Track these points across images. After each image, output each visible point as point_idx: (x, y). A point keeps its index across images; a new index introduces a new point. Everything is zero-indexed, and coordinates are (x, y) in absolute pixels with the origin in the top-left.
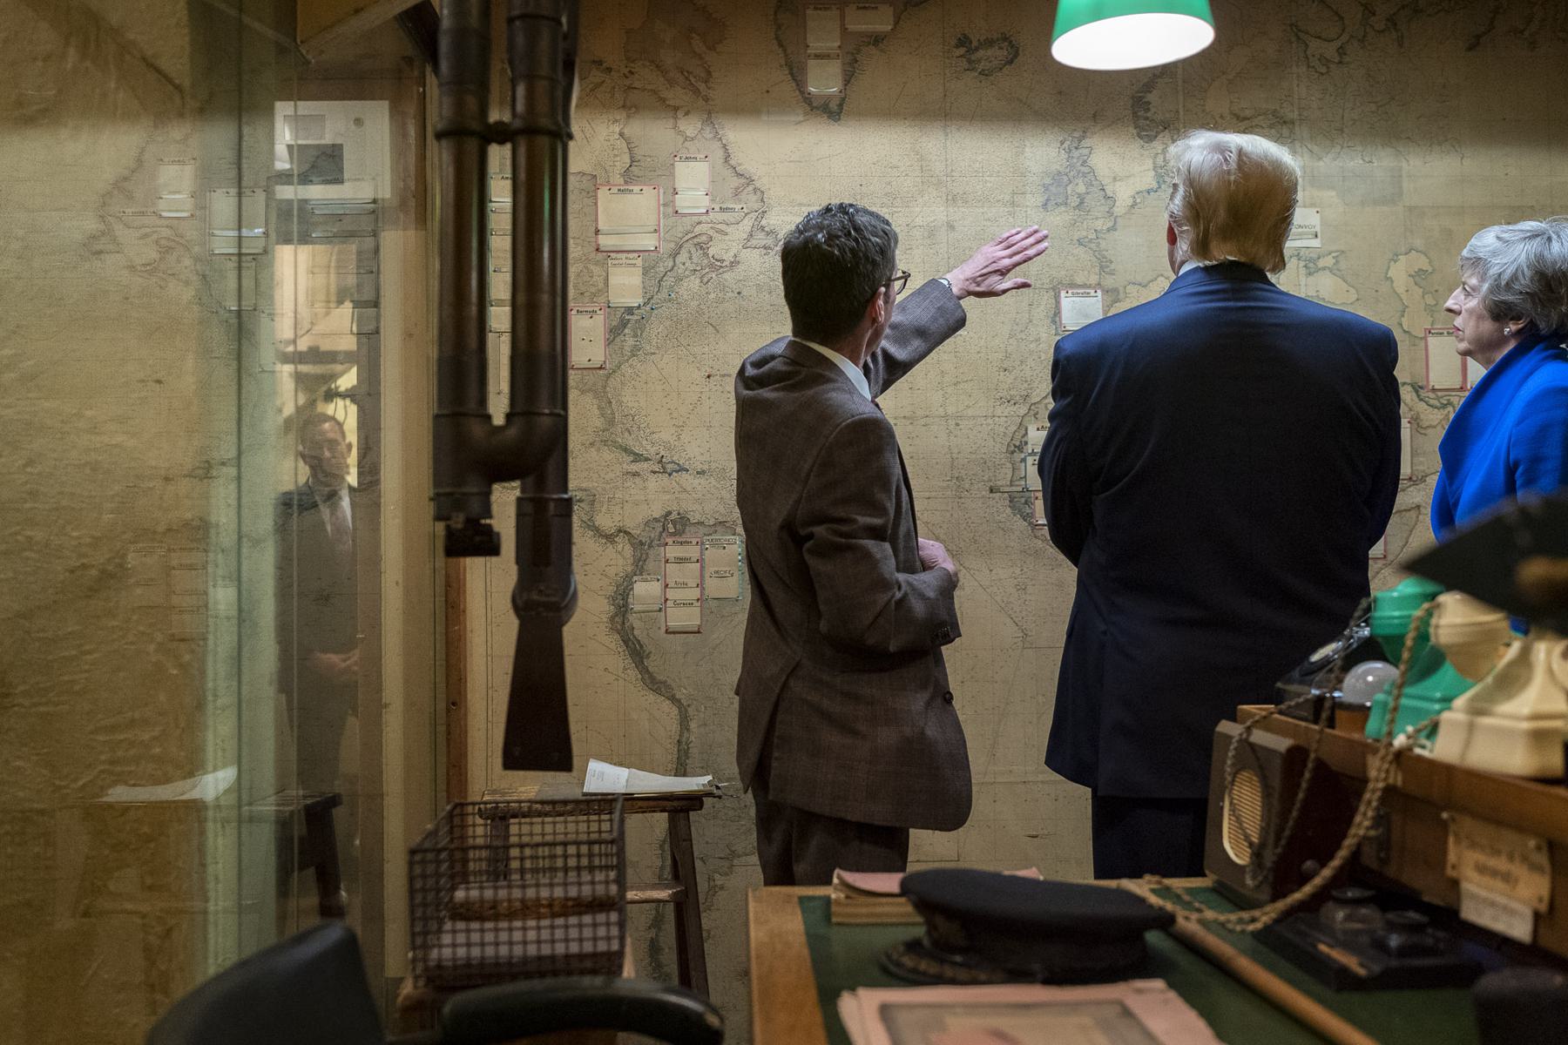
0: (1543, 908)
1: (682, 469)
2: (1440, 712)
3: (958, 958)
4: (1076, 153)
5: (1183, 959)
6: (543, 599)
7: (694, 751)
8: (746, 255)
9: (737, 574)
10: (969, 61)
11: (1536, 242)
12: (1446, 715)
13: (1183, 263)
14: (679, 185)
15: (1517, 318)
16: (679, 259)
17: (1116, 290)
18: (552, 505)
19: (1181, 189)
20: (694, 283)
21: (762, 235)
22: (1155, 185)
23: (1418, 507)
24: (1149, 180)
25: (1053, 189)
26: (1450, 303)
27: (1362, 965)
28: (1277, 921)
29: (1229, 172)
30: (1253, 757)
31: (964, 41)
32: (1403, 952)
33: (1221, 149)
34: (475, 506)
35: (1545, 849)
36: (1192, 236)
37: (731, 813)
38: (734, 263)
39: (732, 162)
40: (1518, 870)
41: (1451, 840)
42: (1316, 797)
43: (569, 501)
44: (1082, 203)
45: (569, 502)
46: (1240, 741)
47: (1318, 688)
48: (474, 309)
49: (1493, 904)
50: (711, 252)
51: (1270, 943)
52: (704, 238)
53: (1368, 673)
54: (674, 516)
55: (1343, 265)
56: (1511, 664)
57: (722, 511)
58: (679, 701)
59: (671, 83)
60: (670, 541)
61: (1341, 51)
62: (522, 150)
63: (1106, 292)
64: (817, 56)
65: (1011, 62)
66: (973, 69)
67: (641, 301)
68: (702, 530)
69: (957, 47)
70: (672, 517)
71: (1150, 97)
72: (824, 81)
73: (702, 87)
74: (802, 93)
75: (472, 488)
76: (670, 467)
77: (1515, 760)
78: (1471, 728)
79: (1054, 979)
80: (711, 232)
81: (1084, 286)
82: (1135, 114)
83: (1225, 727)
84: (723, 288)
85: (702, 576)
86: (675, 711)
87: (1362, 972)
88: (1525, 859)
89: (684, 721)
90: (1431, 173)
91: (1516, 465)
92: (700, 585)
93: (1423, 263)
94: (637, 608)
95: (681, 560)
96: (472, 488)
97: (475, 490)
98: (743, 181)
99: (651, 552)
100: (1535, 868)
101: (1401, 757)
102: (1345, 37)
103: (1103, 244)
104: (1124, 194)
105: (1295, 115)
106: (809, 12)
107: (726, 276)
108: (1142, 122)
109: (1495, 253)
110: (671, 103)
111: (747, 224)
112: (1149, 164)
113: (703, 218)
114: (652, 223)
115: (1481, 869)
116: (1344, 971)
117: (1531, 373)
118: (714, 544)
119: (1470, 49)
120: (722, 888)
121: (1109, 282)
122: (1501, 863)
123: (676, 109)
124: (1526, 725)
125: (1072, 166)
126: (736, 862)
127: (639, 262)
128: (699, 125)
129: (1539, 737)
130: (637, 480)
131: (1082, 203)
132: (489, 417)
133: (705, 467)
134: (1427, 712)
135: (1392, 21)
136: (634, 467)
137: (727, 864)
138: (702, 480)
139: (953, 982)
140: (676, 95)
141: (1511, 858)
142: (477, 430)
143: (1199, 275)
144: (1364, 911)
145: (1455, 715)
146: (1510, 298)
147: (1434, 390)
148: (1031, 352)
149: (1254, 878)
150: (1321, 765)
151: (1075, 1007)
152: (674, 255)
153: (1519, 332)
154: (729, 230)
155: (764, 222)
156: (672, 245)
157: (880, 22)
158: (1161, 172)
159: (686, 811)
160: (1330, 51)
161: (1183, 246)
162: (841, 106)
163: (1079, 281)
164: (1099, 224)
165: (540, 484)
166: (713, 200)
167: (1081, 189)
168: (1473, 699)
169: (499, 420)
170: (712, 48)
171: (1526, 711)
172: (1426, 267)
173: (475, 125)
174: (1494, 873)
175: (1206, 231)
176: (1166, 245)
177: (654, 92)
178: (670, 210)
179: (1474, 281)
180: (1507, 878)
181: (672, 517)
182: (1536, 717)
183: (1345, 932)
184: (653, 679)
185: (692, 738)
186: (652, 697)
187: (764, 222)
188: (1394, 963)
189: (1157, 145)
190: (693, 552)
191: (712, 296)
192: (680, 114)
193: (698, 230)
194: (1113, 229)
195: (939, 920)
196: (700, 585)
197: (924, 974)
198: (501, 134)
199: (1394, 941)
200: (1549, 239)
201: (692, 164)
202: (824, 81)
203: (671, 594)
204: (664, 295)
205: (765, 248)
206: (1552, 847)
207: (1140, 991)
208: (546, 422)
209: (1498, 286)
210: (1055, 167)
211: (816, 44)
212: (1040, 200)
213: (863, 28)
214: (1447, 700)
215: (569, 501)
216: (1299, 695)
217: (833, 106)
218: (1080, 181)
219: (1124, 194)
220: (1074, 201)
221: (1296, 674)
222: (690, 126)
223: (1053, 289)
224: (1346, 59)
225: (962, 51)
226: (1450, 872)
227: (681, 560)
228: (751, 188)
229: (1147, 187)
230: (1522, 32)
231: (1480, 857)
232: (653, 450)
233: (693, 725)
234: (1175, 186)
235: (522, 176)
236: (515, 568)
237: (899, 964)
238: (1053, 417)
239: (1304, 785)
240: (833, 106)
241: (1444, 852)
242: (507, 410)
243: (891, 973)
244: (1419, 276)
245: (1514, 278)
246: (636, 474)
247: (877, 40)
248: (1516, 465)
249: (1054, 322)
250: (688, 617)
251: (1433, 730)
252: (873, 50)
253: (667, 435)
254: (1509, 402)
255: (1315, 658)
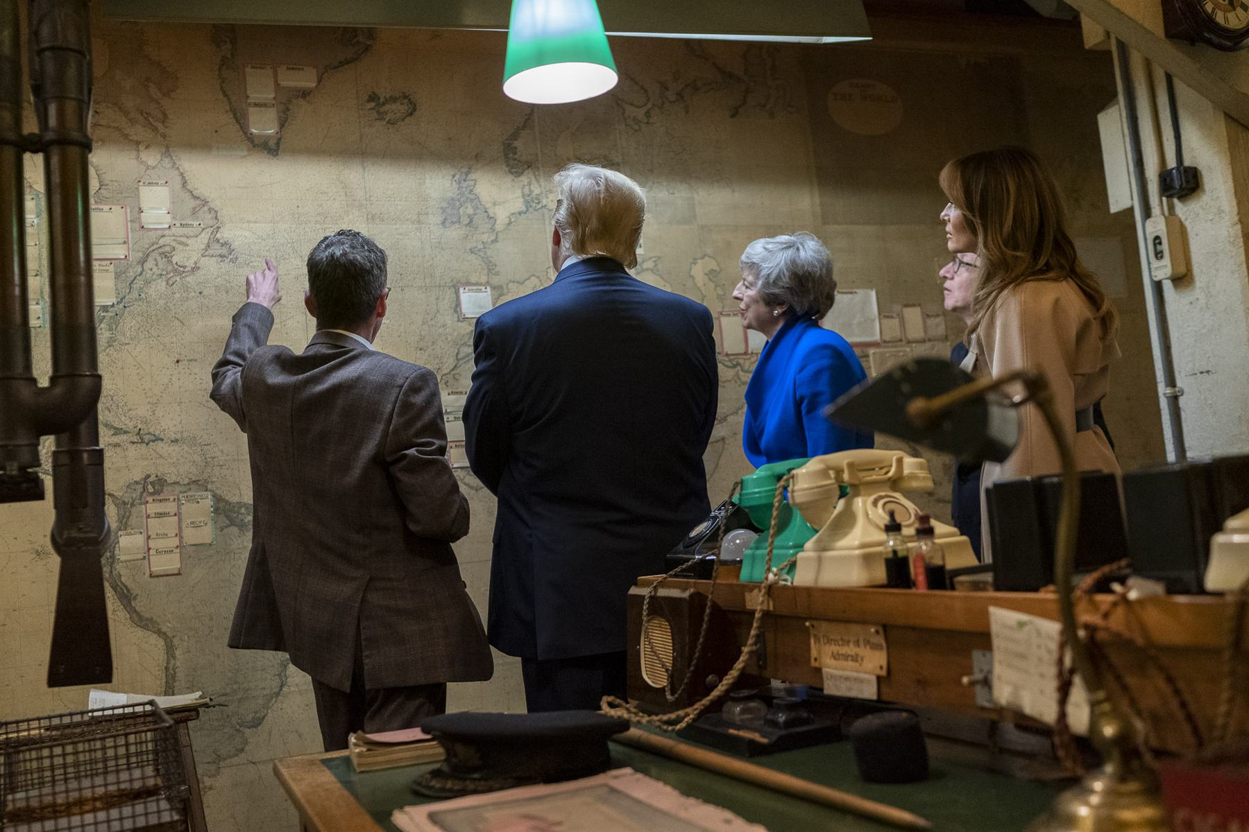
0: (884, 673)
1: (158, 439)
2: (796, 554)
3: (476, 776)
4: (464, 184)
5: (636, 754)
6: (82, 535)
7: (180, 675)
8: (204, 262)
9: (210, 523)
10: (378, 113)
11: (790, 252)
12: (800, 555)
13: (566, 258)
14: (144, 206)
15: (781, 304)
16: (148, 265)
17: (500, 287)
18: (85, 456)
19: (565, 205)
20: (161, 285)
21: (218, 246)
22: (524, 208)
23: (723, 439)
24: (519, 205)
25: (449, 211)
26: (736, 293)
27: (764, 737)
28: (699, 716)
29: (599, 192)
30: (659, 607)
31: (373, 98)
32: (788, 724)
33: (594, 177)
34: (25, 457)
35: (881, 632)
36: (573, 236)
37: (216, 724)
38: (195, 269)
39: (189, 187)
40: (864, 651)
41: (812, 641)
42: (713, 631)
43: (102, 450)
44: (471, 221)
45: (100, 453)
46: (651, 597)
47: (699, 554)
48: (17, 291)
49: (847, 679)
50: (175, 260)
51: (692, 734)
52: (167, 249)
53: (736, 537)
54: (152, 478)
55: (660, 266)
56: (840, 514)
57: (194, 470)
58: (165, 634)
59: (133, 122)
60: (150, 499)
61: (648, 114)
62: (55, 160)
63: (494, 288)
64: (256, 105)
65: (411, 114)
66: (383, 119)
67: (115, 301)
68: (178, 489)
69: (369, 101)
70: (151, 479)
71: (516, 144)
72: (264, 125)
73: (160, 126)
74: (245, 133)
75: (22, 441)
76: (146, 438)
77: (854, 576)
78: (820, 560)
79: (549, 779)
80: (173, 244)
81: (476, 284)
82: (506, 155)
83: (634, 591)
84: (186, 289)
85: (180, 528)
86: (161, 643)
87: (765, 741)
88: (867, 642)
89: (170, 650)
90: (714, 202)
91: (802, 399)
92: (179, 535)
93: (713, 265)
94: (123, 558)
95: (160, 515)
96: (22, 441)
97: (25, 442)
98: (198, 202)
99: (134, 510)
100: (875, 647)
101: (771, 590)
102: (649, 106)
103: (489, 253)
104: (502, 214)
105: (619, 159)
106: (248, 70)
107: (188, 279)
108: (511, 162)
109: (764, 260)
110: (135, 138)
111: (204, 237)
112: (519, 193)
113: (166, 232)
114: (121, 236)
115: (836, 657)
116: (752, 742)
117: (799, 338)
118: (189, 499)
119: (733, 116)
120: (210, 788)
121: (495, 281)
122: (851, 650)
123: (138, 143)
124: (857, 552)
125: (462, 194)
126: (222, 764)
127: (111, 268)
128: (159, 157)
129: (868, 559)
130: (118, 450)
131: (471, 221)
132: (34, 381)
133: (178, 436)
134: (786, 556)
135: (680, 95)
136: (116, 439)
137: (213, 767)
138: (176, 448)
139: (475, 792)
140: (138, 132)
141: (857, 644)
142: (25, 392)
143: (581, 268)
144: (752, 704)
145: (809, 551)
146: (776, 291)
147: (727, 355)
148: (440, 335)
149: (672, 694)
150: (715, 607)
151: (576, 792)
152: (142, 262)
153: (784, 313)
154: (189, 242)
155: (218, 236)
156: (140, 254)
157: (305, 79)
158: (531, 203)
159: (186, 720)
160: (640, 113)
161: (566, 244)
162: (278, 144)
163: (473, 280)
164: (485, 237)
165: (75, 438)
166: (174, 218)
167: (470, 211)
168: (818, 541)
169: (44, 382)
170: (167, 94)
171: (857, 543)
172: (716, 268)
173: (11, 135)
174: (846, 657)
175: (584, 232)
176: (550, 245)
177: (118, 129)
178: (137, 226)
179: (750, 278)
180: (855, 658)
181: (151, 479)
182: (863, 546)
183: (742, 721)
184: (140, 617)
185: (178, 664)
186: (140, 633)
187: (218, 236)
188: (783, 732)
189: (524, 179)
190: (171, 507)
191: (178, 295)
192: (141, 147)
193: (162, 242)
194: (495, 241)
195: (460, 749)
196: (179, 535)
197: (451, 790)
198: (35, 145)
199: (782, 718)
200: (798, 249)
201: (154, 188)
202: (264, 125)
203: (152, 544)
204: (135, 295)
205: (221, 256)
206: (886, 629)
207: (616, 777)
208: (87, 382)
209: (768, 283)
210: (450, 195)
211: (254, 96)
212: (439, 219)
213: (291, 84)
214: (799, 547)
215: (102, 450)
216: (688, 560)
217: (272, 143)
218: (469, 205)
219: (502, 214)
220: (466, 220)
221: (681, 547)
222: (151, 157)
223: (454, 286)
224: (651, 120)
225: (373, 104)
226: (813, 664)
227: (160, 515)
228: (206, 208)
229: (517, 210)
230: (764, 106)
231: (834, 648)
232: (131, 425)
233: (177, 653)
234: (560, 202)
235: (56, 179)
236: (53, 511)
237: (431, 788)
238: (475, 377)
239: (706, 618)
240: (272, 143)
241: (809, 650)
242: (50, 373)
243: (420, 794)
244: (711, 274)
245: (778, 278)
246: (117, 445)
247: (305, 94)
248: (802, 399)
249: (456, 311)
250: (171, 563)
251: (792, 566)
252: (301, 101)
253: (143, 411)
254: (790, 357)
255: (693, 534)
